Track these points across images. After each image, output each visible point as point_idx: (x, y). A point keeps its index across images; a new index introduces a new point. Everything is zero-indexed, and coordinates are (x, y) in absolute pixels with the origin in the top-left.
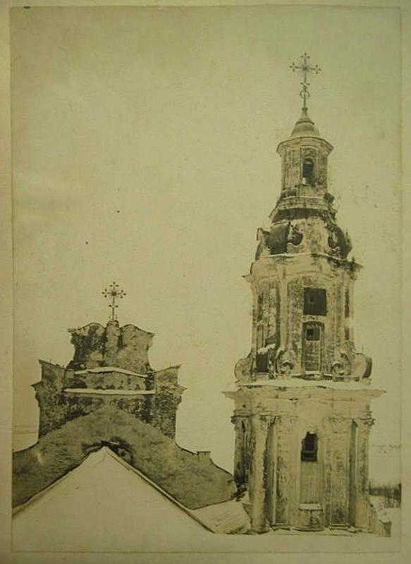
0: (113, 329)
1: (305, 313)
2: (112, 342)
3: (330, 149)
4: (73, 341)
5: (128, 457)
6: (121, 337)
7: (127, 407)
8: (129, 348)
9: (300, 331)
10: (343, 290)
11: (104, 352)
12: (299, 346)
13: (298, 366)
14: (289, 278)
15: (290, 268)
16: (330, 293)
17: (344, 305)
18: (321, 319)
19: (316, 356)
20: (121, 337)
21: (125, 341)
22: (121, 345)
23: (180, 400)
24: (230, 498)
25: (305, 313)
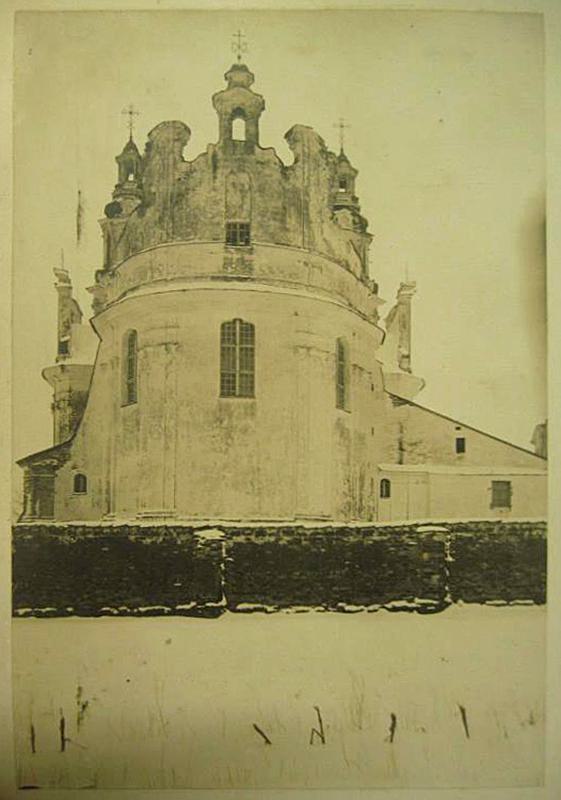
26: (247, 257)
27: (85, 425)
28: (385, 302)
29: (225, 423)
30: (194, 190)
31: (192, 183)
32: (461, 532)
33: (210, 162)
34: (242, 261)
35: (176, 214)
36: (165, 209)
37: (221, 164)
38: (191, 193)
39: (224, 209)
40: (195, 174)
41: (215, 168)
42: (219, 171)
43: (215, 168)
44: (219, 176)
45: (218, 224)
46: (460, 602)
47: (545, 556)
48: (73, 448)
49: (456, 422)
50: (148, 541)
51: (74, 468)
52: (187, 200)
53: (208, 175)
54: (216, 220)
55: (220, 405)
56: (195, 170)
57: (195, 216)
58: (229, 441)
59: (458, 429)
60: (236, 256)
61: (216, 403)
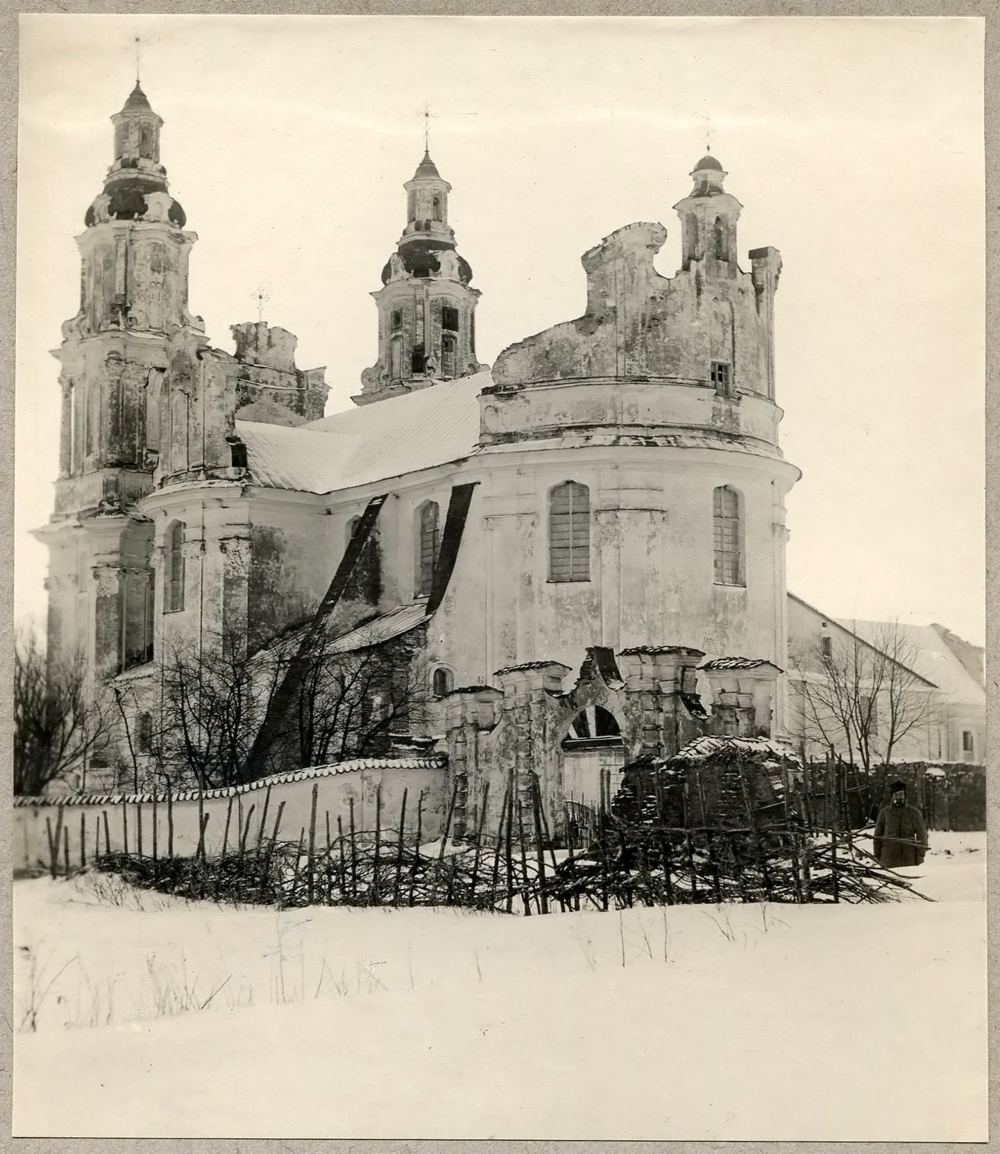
0: (262, 330)
1: (444, 327)
2: (263, 341)
3: (449, 188)
4: (235, 337)
5: (712, 208)
6: (269, 337)
7: (282, 400)
8: (277, 348)
9: (440, 342)
10: (469, 312)
11: (256, 349)
12: (440, 355)
13: (439, 370)
14: (431, 298)
15: (432, 290)
16: (460, 312)
17: (469, 324)
18: (454, 333)
19: (451, 364)
20: (269, 337)
21: (273, 341)
22: (270, 345)
23: (327, 398)
24: (30, 963)
25: (444, 327)
26: (734, 408)
27: (449, 600)
28: (138, 99)
29: (720, 617)
30: (673, 315)
31: (670, 306)
32: (591, 867)
33: (693, 283)
34: (730, 413)
35: (649, 342)
36: (635, 332)
37: (704, 288)
38: (669, 321)
39: (708, 345)
40: (674, 295)
41: (699, 292)
42: (703, 296)
43: (699, 292)
44: (703, 302)
45: (703, 364)
46: (937, 839)
47: (983, 802)
48: (430, 631)
49: (823, 616)
50: (705, 745)
51: (433, 659)
52: (665, 327)
53: (691, 299)
54: (700, 358)
55: (714, 592)
56: (675, 290)
57: (677, 350)
58: (725, 641)
59: (824, 625)
60: (725, 407)
61: (710, 592)
